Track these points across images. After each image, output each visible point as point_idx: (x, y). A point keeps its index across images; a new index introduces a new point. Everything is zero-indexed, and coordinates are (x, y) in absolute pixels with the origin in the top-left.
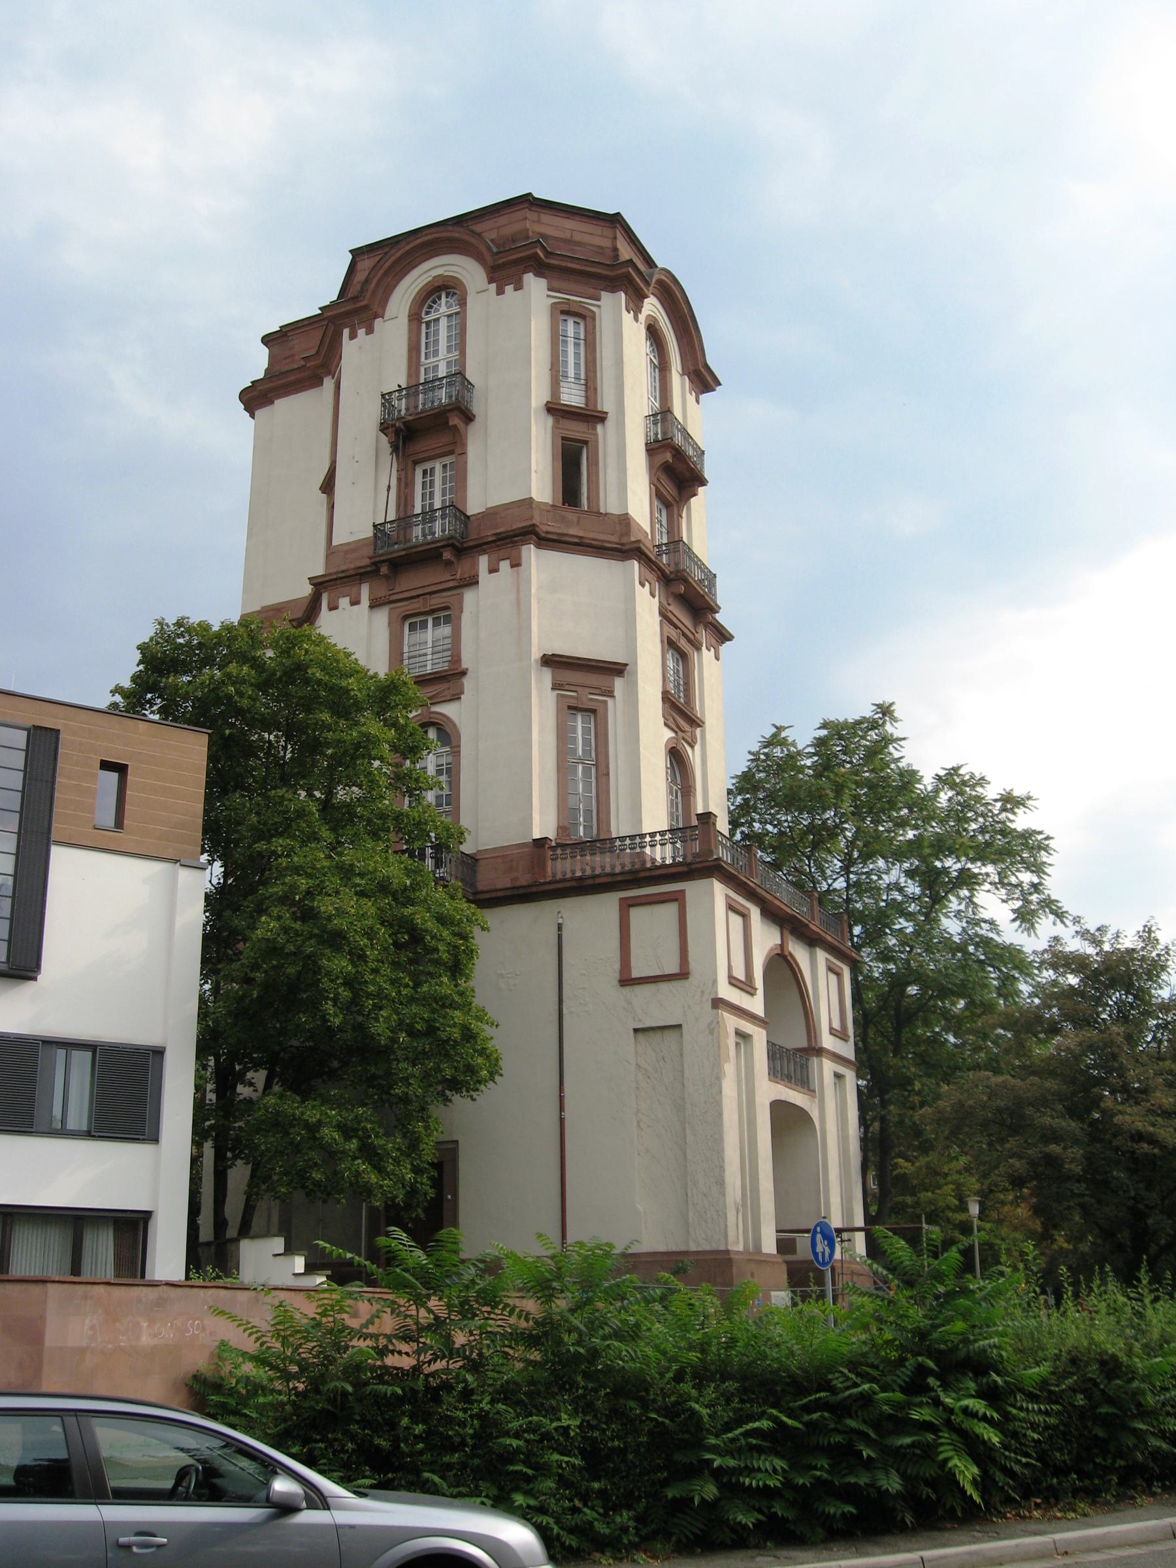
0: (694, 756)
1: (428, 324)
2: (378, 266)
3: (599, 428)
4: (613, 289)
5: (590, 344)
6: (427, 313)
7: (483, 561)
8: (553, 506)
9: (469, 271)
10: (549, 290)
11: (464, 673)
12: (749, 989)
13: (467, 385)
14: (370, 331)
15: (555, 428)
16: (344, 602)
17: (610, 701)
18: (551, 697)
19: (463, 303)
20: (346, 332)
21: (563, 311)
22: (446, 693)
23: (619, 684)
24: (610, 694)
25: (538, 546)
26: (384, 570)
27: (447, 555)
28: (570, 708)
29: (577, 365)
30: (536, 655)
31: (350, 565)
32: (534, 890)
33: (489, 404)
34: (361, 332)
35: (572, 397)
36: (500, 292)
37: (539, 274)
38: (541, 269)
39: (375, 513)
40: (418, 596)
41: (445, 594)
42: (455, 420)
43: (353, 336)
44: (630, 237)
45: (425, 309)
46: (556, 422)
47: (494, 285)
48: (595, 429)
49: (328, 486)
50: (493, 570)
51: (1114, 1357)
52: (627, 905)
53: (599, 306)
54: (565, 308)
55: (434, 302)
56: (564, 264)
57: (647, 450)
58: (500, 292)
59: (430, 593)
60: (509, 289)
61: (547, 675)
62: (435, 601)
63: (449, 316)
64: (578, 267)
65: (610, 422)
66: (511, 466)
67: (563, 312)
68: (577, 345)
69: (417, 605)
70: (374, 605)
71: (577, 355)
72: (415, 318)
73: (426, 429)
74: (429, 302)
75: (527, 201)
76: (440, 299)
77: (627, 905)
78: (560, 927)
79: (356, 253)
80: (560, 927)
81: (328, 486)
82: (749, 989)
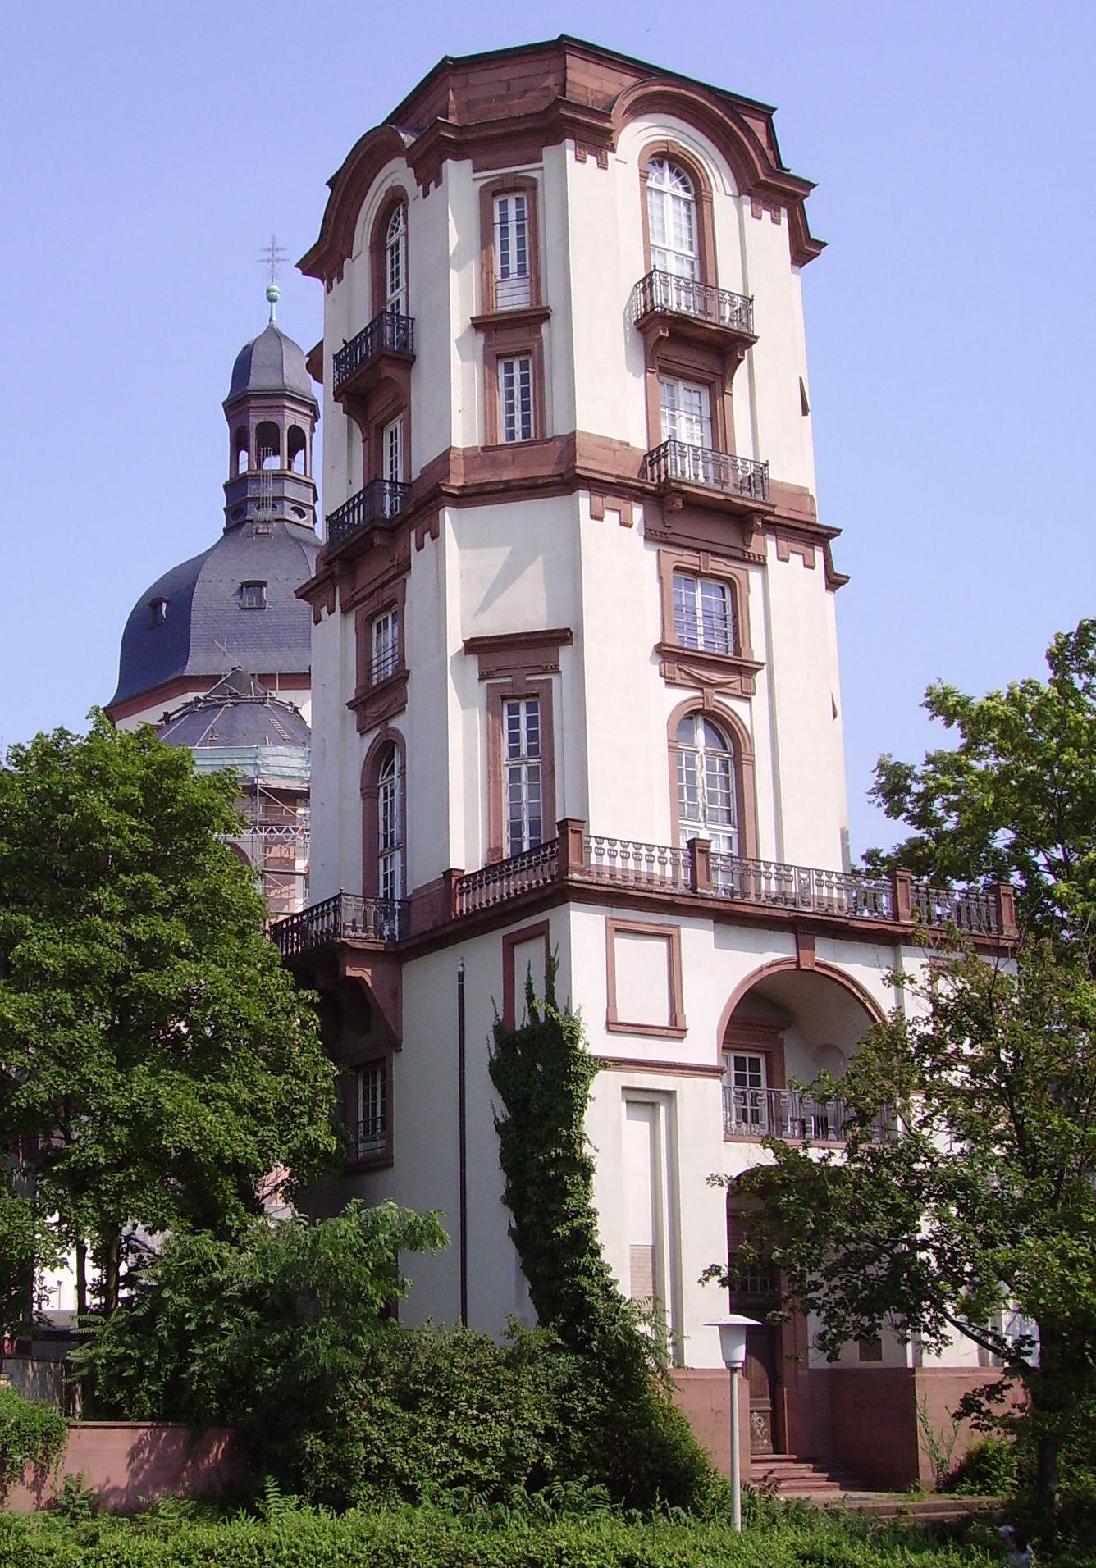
2: (348, 186)
3: (544, 328)
8: (483, 449)
17: (554, 678)
18: (479, 690)
21: (491, 193)
23: (565, 654)
25: (458, 506)
32: (441, 932)
37: (458, 157)
38: (459, 151)
40: (371, 594)
42: (388, 371)
44: (597, 56)
48: (539, 331)
51: (405, 1500)
52: (510, 944)
54: (498, 186)
56: (484, 134)
57: (638, 329)
59: (382, 586)
65: (555, 319)
70: (344, 612)
75: (448, 69)
78: (461, 976)
80: (461, 976)
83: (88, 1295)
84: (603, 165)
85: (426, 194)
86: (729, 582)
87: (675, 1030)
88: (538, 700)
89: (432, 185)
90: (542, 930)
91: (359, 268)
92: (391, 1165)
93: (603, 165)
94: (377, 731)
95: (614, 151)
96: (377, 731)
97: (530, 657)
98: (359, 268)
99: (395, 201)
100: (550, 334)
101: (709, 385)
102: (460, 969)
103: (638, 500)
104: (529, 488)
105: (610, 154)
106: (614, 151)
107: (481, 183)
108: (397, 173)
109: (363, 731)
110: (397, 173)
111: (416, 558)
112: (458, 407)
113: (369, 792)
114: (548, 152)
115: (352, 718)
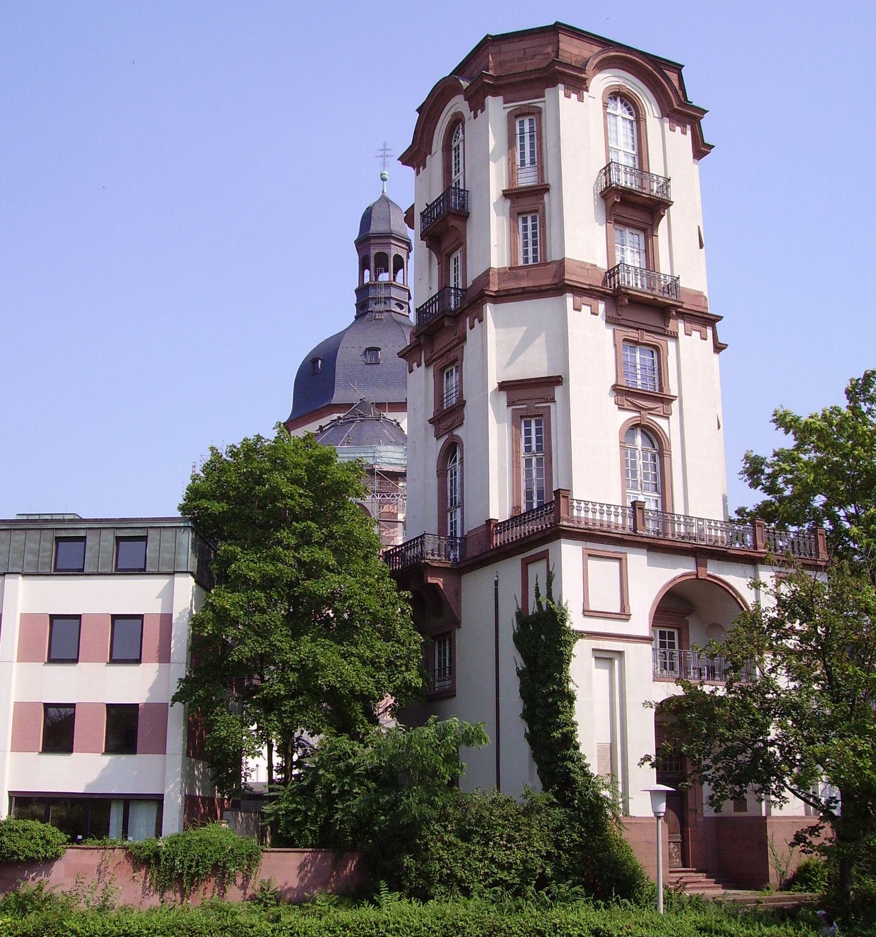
0: (668, 427)
2: (429, 112)
3: (546, 197)
5: (538, 135)
8: (510, 268)
10: (505, 103)
12: (623, 617)
17: (552, 405)
23: (558, 391)
30: (492, 385)
32: (484, 557)
40: (443, 355)
42: (453, 222)
44: (577, 34)
46: (512, 202)
48: (543, 199)
51: (463, 895)
52: (526, 564)
54: (518, 112)
56: (510, 81)
59: (449, 350)
61: (503, 396)
64: (518, 79)
65: (553, 191)
70: (427, 366)
75: (489, 42)
77: (526, 564)
78: (496, 583)
80: (496, 583)
82: (623, 617)
83: (274, 773)
84: (581, 99)
85: (475, 116)
86: (656, 348)
87: (624, 615)
88: (543, 419)
89: (479, 111)
90: (545, 556)
91: (435, 161)
92: (455, 695)
93: (581, 99)
94: (446, 437)
95: (587, 91)
96: (446, 437)
97: (538, 392)
98: (435, 161)
99: (457, 121)
100: (550, 200)
101: (644, 230)
102: (496, 579)
103: (602, 299)
104: (537, 292)
105: (585, 93)
106: (587, 91)
107: (509, 110)
108: (458, 104)
109: (438, 437)
110: (458, 104)
111: (469, 333)
112: (495, 244)
113: (442, 473)
114: (548, 92)
115: (431, 429)
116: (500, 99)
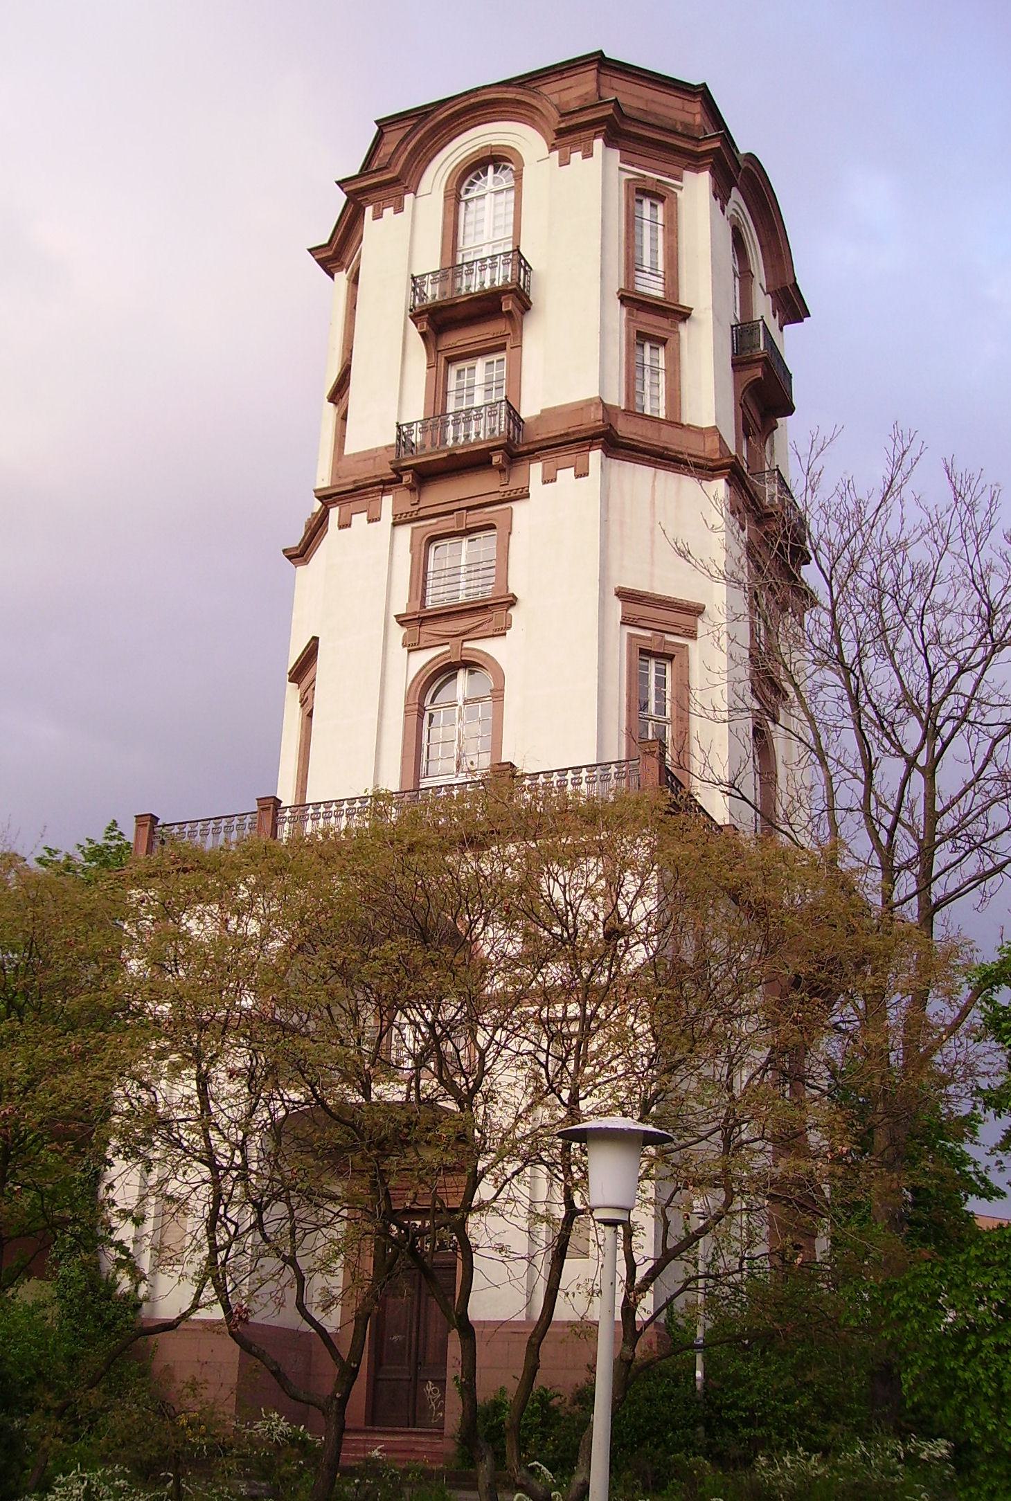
1: (467, 202)
4: (697, 169)
6: (467, 191)
7: (536, 470)
9: (523, 138)
11: (512, 602)
13: (527, 268)
14: (399, 209)
15: (628, 320)
16: (360, 520)
19: (518, 177)
20: (369, 211)
21: (641, 192)
22: (485, 627)
24: (692, 635)
26: (407, 478)
27: (497, 459)
28: (642, 652)
29: (654, 252)
31: (365, 473)
33: (546, 294)
34: (389, 212)
35: (653, 288)
36: (564, 162)
39: (619, 753)
40: (451, 512)
41: (487, 510)
43: (378, 216)
45: (465, 186)
46: (629, 313)
47: (556, 153)
48: (676, 326)
49: (339, 392)
50: (548, 479)
53: (681, 188)
55: (478, 178)
58: (564, 162)
59: (468, 509)
60: (576, 157)
62: (474, 518)
63: (496, 193)
66: (565, 361)
67: (639, 191)
68: (654, 230)
69: (449, 524)
71: (654, 240)
72: (455, 198)
73: (469, 317)
74: (470, 178)
76: (485, 173)
79: (384, 124)
81: (339, 392)
116: (615, 154)
